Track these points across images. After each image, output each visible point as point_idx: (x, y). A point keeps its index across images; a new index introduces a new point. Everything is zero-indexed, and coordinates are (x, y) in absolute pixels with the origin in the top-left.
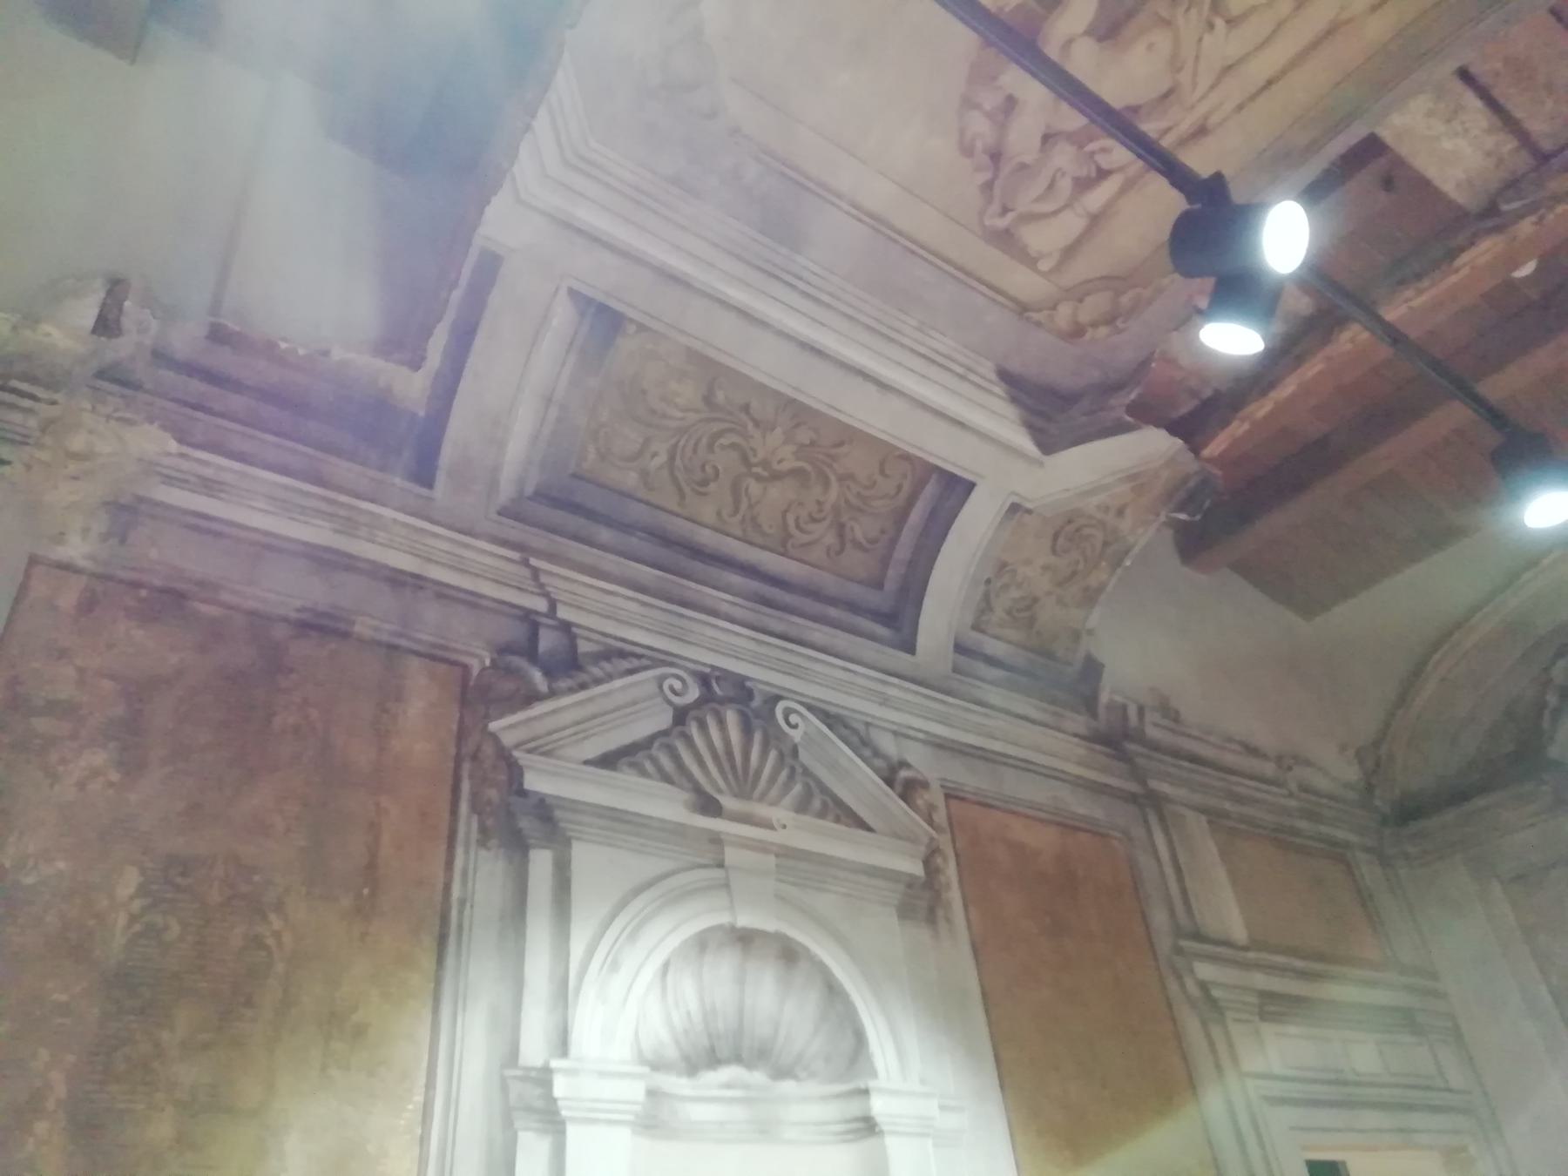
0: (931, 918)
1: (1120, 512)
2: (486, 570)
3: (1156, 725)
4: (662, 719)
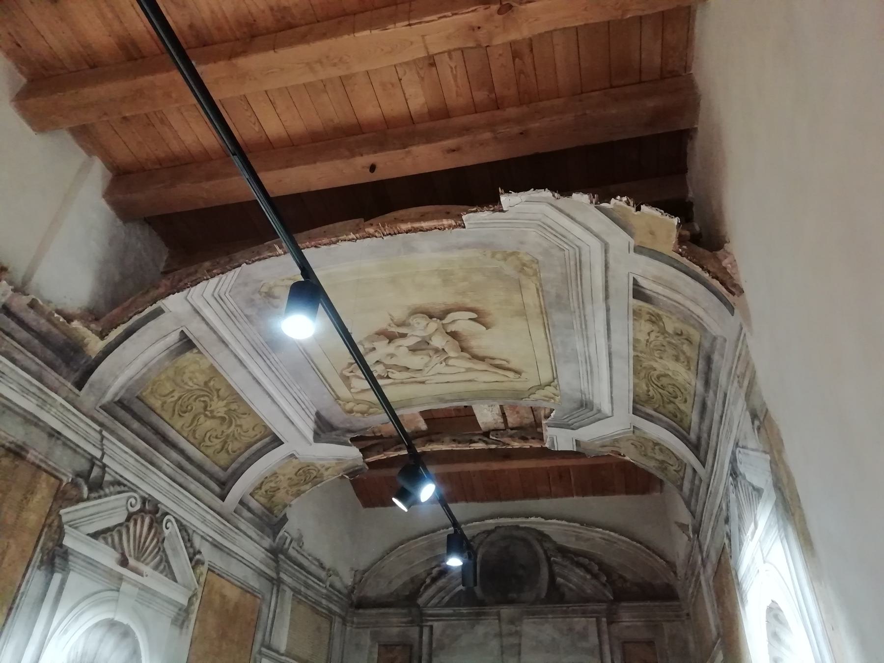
0: (181, 627)
1: (327, 469)
2: (82, 432)
4: (122, 519)
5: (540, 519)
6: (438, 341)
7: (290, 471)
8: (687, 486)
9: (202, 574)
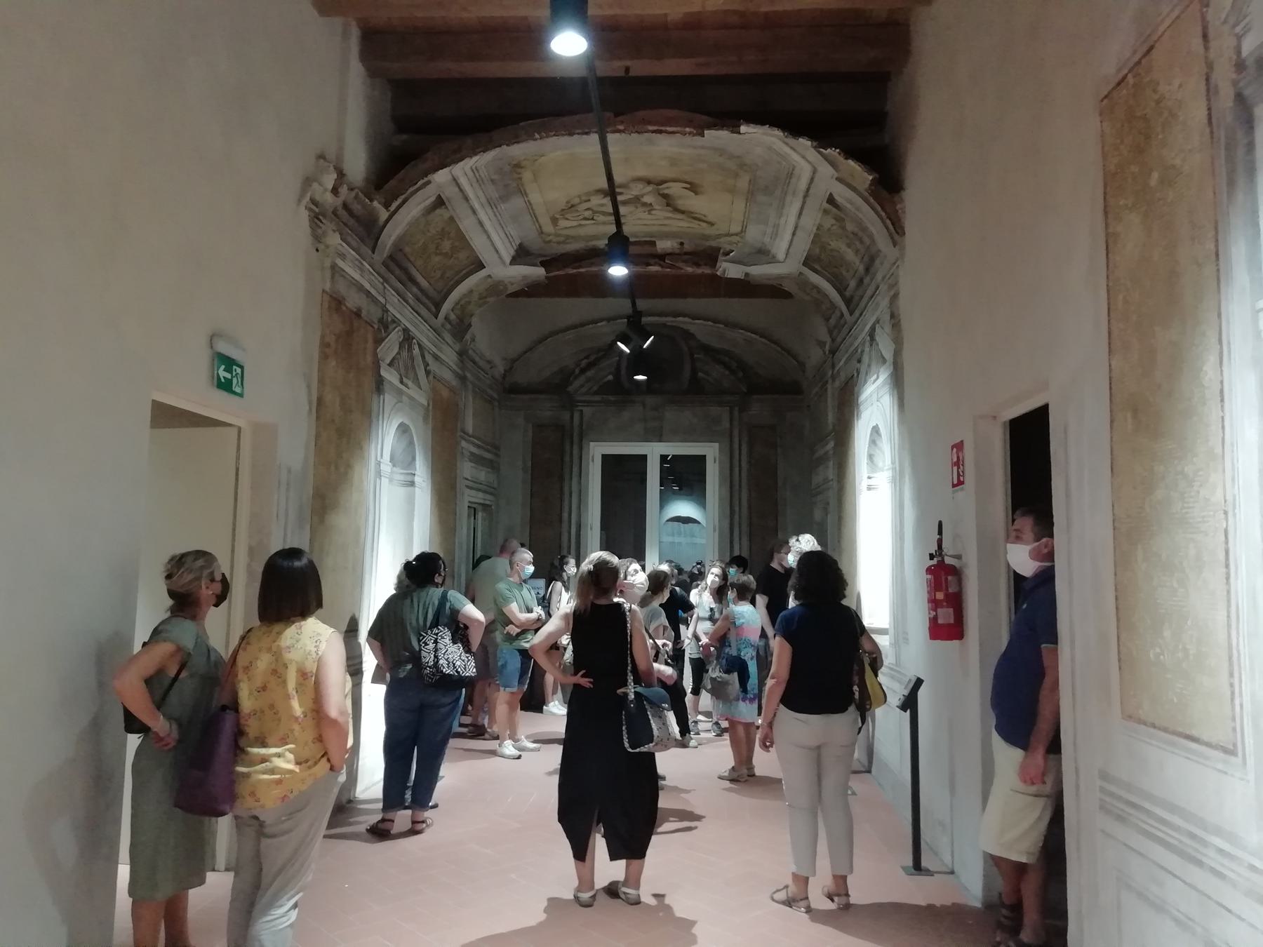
5: (686, 319)
8: (833, 321)
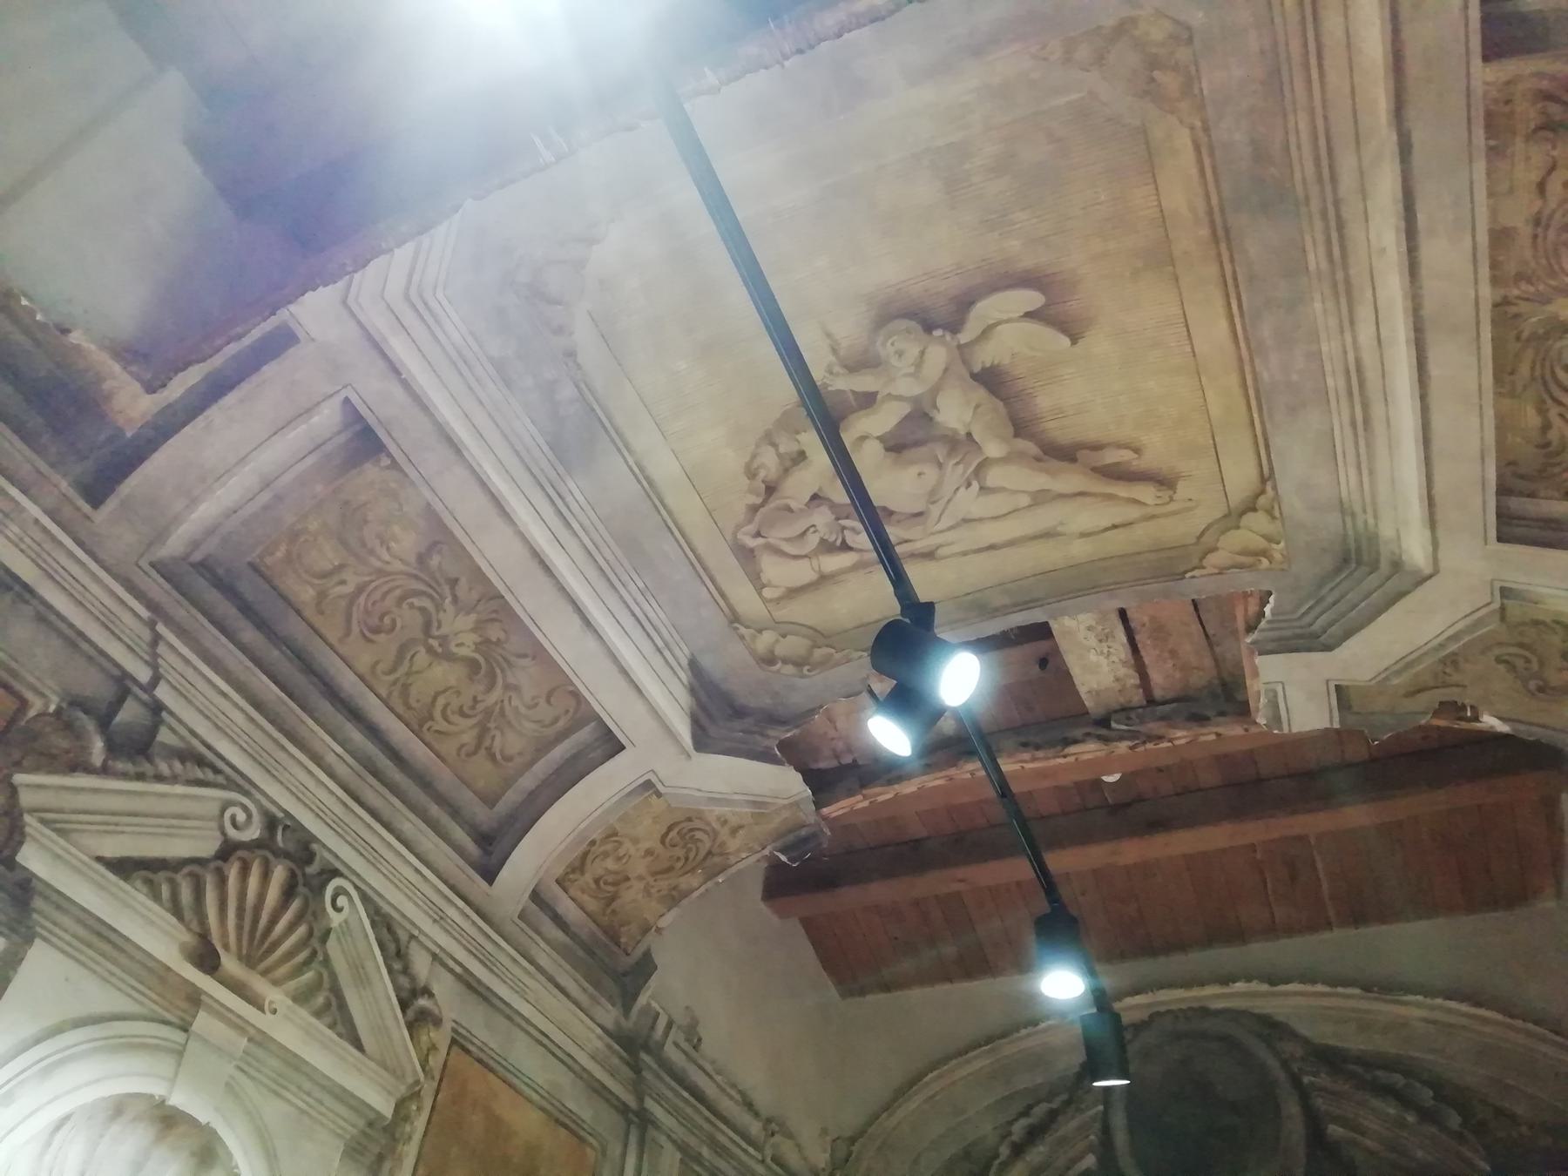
1: (734, 831)
3: (676, 1045)
4: (207, 847)
5: (1256, 986)
6: (956, 411)
7: (647, 831)
9: (433, 1047)
